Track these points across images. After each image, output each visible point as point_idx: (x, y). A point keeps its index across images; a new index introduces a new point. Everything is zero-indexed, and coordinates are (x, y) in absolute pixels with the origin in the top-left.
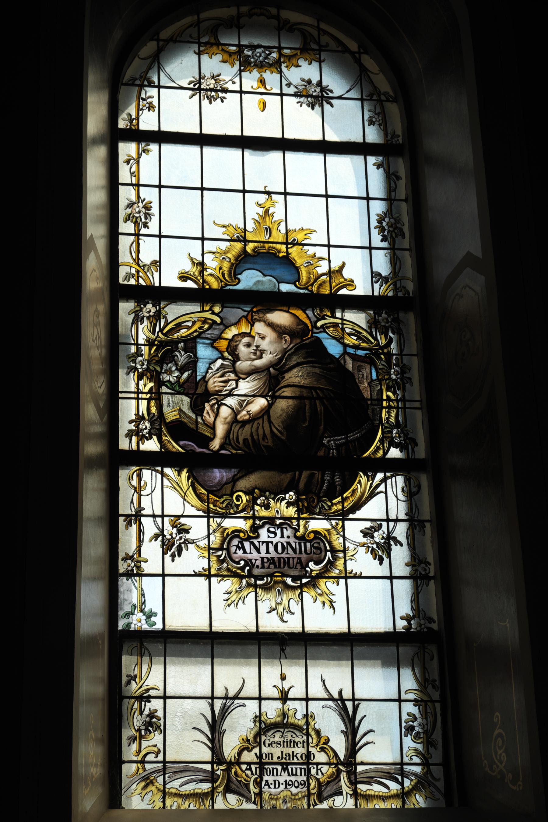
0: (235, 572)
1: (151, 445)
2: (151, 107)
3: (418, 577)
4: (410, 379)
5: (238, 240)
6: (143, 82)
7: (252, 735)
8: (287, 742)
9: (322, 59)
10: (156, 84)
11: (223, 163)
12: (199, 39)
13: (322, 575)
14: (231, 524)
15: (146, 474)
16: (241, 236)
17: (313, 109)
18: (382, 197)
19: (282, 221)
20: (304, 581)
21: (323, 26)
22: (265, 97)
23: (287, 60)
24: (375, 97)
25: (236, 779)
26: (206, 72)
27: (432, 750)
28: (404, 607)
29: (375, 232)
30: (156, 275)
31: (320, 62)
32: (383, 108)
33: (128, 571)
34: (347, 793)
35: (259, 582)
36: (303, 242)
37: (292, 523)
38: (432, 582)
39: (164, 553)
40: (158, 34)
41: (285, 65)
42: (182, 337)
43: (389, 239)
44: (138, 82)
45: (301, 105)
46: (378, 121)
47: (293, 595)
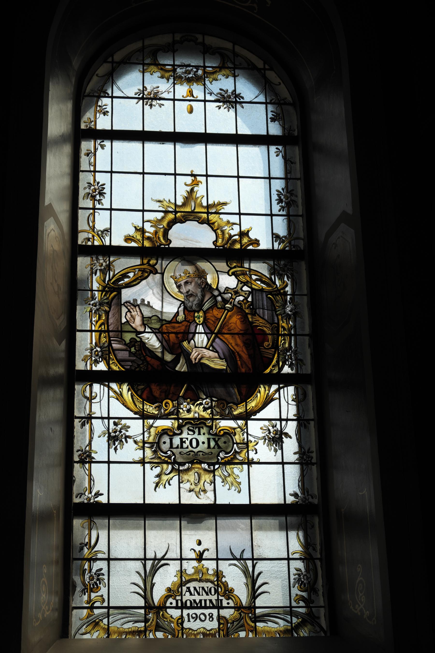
1: (102, 367)
2: (105, 113)
3: (304, 460)
9: (236, 74)
10: (110, 95)
11: (159, 155)
15: (96, 387)
22: (192, 103)
28: (293, 486)
29: (274, 203)
30: (107, 239)
31: (235, 76)
35: (181, 468)
38: (314, 468)
45: (220, 108)
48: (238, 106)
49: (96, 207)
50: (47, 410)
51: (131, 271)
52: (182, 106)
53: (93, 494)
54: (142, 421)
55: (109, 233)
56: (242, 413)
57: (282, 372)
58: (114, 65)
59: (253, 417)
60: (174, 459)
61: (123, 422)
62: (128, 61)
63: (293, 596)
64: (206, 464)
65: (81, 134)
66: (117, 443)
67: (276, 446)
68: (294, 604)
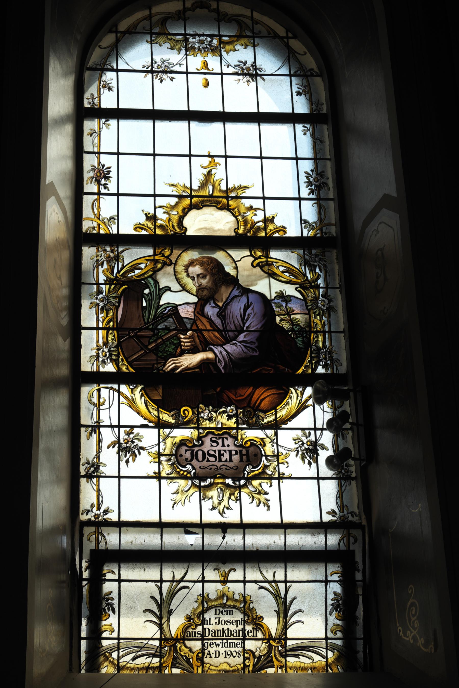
1: (110, 368)
9: (256, 44)
10: (115, 68)
11: (172, 134)
13: (256, 477)
18: (310, 157)
21: (256, 15)
22: (207, 76)
26: (157, 58)
28: (330, 503)
32: (308, 82)
35: (203, 484)
40: (116, 26)
48: (258, 78)
49: (101, 192)
53: (102, 510)
54: (157, 430)
55: (116, 221)
56: (271, 421)
58: (119, 35)
59: (283, 426)
60: (194, 473)
61: (136, 431)
62: (133, 31)
63: (330, 626)
64: (230, 479)
65: (83, 113)
66: (128, 455)
67: (311, 458)
68: (330, 635)
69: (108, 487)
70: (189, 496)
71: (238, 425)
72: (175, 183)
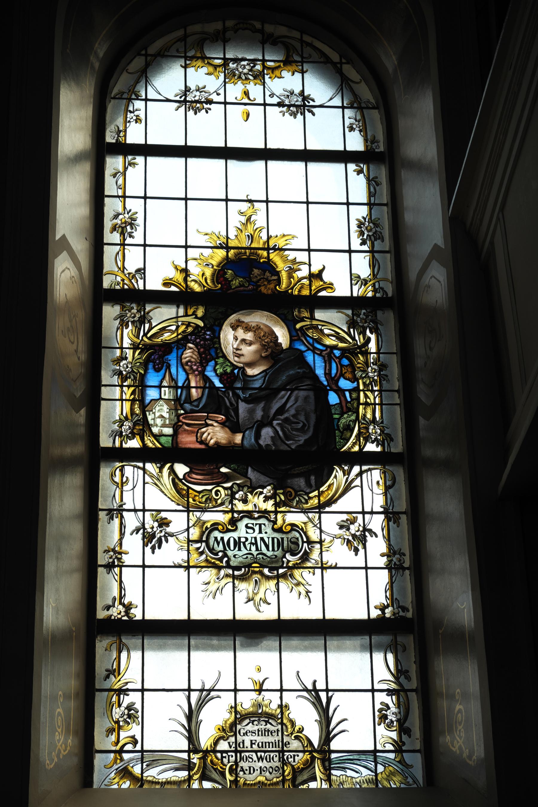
0: (214, 563)
1: (134, 443)
2: (138, 120)
4: (387, 376)
5: (220, 247)
6: (131, 95)
7: (228, 725)
8: (262, 731)
9: (305, 70)
10: (144, 97)
11: (207, 174)
12: (185, 53)
13: (296, 566)
14: (210, 517)
15: (129, 470)
16: (223, 243)
17: (295, 117)
19: (264, 228)
20: (281, 571)
22: (248, 107)
23: (270, 71)
24: (355, 105)
25: (212, 767)
26: (192, 85)
27: (405, 738)
28: (379, 597)
29: (354, 236)
30: (141, 282)
31: (303, 72)
32: (363, 116)
33: (109, 563)
34: (321, 779)
35: (236, 573)
36: (283, 247)
37: (270, 516)
38: (407, 572)
39: (145, 545)
41: (269, 76)
42: (166, 340)
43: (368, 242)
44: (125, 96)
45: (284, 115)
46: (359, 127)
47: (272, 584)
50: (63, 500)
51: (171, 324)
52: (235, 112)
57: (365, 450)
58: (149, 58)
65: (103, 148)
68: (379, 747)
69: (131, 577)
70: (220, 588)
71: (276, 509)
72: (209, 232)
